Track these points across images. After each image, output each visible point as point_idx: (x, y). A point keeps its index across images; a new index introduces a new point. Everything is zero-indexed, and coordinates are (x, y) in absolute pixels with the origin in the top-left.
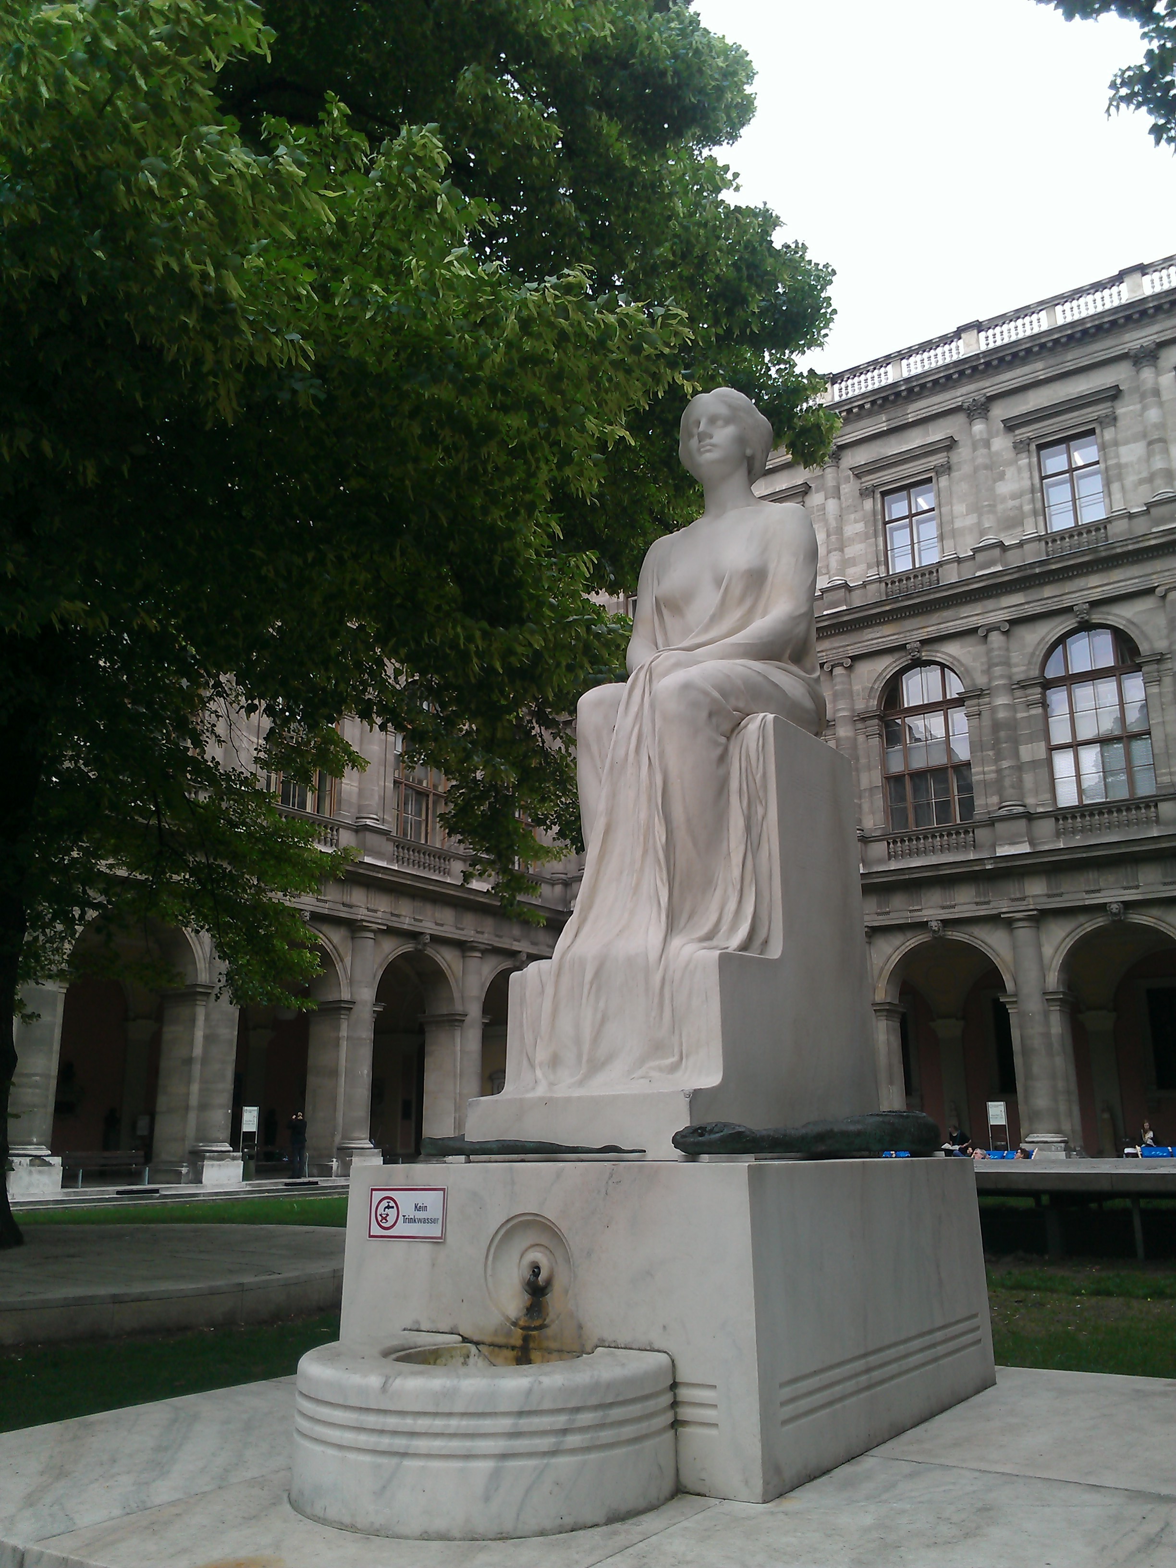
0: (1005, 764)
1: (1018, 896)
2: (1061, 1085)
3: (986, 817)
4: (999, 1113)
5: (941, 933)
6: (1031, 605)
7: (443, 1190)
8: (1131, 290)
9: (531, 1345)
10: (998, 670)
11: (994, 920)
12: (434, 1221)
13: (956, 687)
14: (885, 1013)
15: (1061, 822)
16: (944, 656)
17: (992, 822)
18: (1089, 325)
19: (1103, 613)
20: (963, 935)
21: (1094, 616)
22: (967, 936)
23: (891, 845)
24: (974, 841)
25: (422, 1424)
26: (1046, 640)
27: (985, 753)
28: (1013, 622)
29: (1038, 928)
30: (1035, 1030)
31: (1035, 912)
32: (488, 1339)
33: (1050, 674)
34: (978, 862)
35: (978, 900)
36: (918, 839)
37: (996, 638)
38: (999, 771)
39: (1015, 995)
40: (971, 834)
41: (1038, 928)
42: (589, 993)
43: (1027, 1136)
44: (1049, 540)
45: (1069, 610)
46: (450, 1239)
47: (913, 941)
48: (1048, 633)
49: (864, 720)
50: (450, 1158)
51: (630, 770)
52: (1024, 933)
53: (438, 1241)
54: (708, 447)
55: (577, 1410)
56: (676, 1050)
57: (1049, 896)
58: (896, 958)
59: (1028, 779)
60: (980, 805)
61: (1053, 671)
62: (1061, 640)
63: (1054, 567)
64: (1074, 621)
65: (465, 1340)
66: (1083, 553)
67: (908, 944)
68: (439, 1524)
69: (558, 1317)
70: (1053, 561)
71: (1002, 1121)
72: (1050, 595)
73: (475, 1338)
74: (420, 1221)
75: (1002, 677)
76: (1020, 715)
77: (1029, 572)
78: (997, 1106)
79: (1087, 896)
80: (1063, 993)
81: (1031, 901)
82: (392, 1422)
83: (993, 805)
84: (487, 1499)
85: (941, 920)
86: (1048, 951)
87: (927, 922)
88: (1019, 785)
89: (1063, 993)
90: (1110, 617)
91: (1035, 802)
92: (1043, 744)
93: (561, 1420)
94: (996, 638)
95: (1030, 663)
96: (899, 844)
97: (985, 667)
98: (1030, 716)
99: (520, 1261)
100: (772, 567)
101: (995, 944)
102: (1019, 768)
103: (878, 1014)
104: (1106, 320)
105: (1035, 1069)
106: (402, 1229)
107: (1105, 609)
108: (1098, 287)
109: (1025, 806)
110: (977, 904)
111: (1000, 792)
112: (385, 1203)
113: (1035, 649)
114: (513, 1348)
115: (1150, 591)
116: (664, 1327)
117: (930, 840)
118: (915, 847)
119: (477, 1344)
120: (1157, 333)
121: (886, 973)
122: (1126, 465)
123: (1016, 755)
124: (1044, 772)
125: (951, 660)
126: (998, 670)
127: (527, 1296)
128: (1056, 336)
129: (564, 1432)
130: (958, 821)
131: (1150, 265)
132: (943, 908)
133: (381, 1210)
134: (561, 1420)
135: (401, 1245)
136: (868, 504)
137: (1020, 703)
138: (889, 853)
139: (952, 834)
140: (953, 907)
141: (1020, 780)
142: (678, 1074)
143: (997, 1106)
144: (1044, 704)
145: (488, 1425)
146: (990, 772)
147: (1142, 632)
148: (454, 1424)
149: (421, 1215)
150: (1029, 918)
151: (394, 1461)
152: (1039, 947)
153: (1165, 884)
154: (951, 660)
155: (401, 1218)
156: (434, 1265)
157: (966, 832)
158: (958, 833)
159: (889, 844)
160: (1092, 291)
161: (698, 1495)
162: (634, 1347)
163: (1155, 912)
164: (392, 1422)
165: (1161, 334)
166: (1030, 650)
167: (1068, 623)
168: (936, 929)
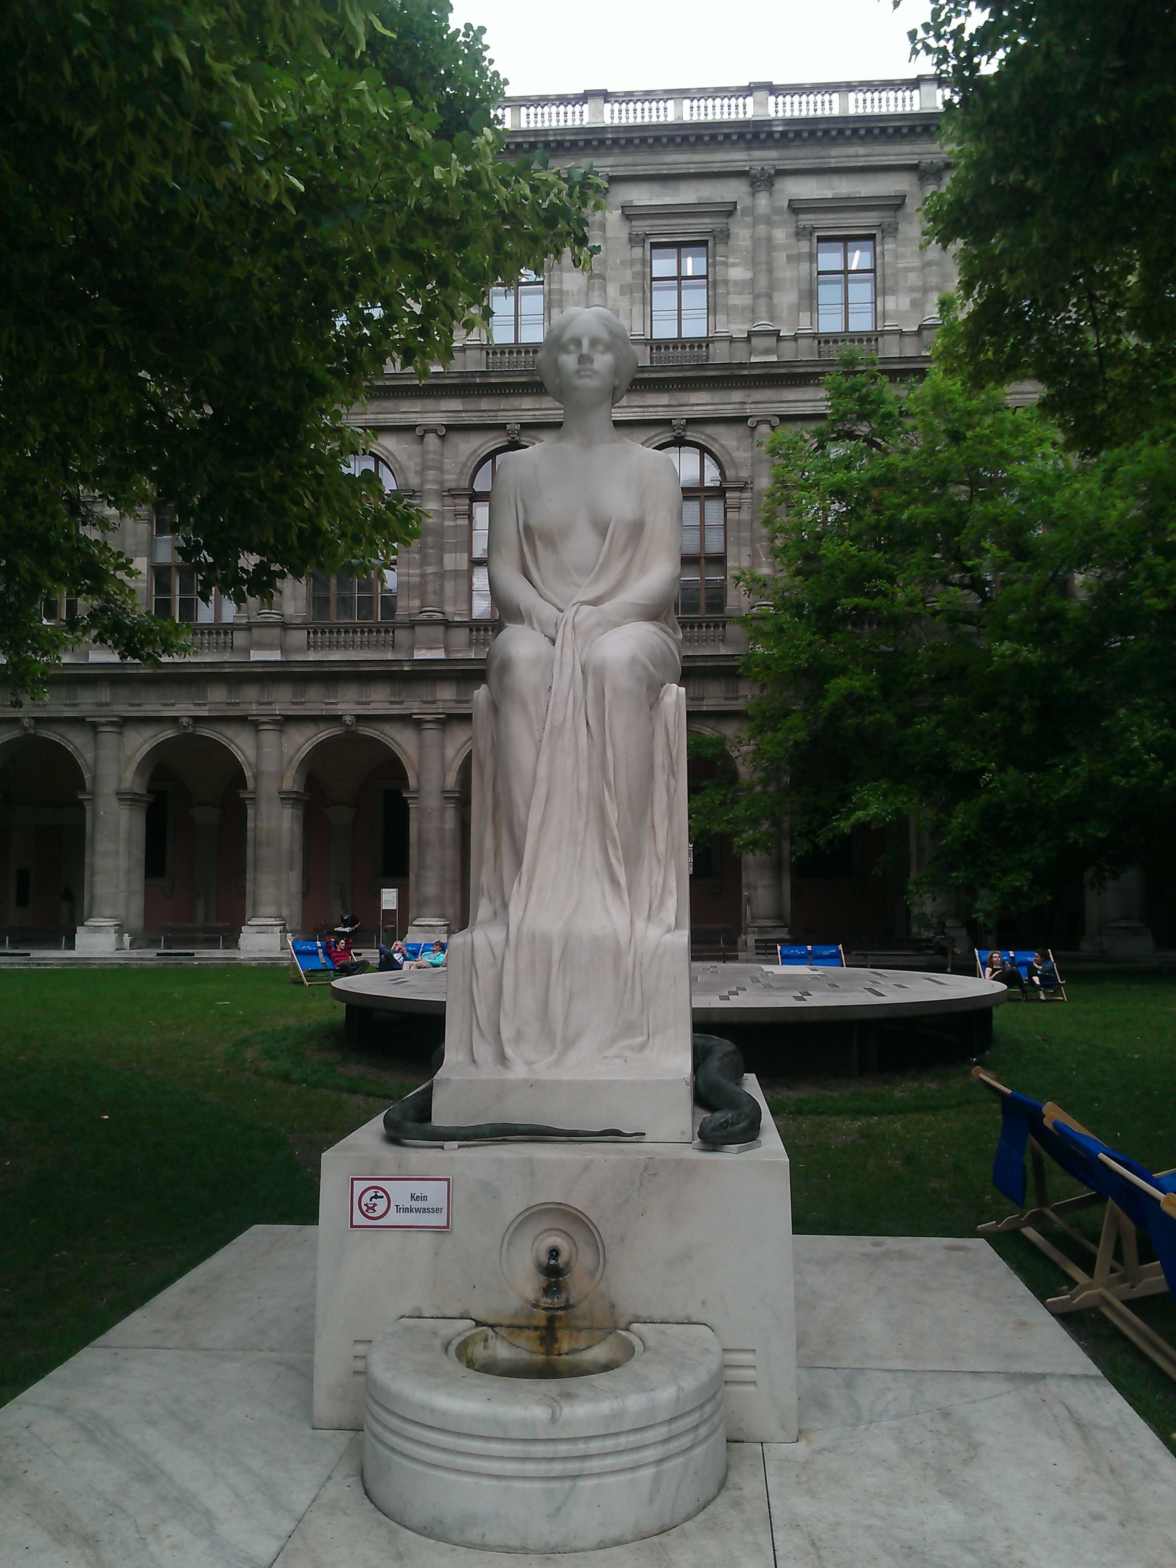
0: (430, 570)
1: (430, 699)
3: (407, 620)
4: (391, 899)
6: (469, 414)
7: (448, 1180)
8: (592, 114)
9: (557, 1325)
10: (431, 474)
11: (405, 719)
12: (438, 1210)
14: (292, 802)
15: (474, 633)
16: (379, 448)
17: (412, 625)
18: (551, 138)
19: (702, 433)
21: (523, 439)
22: (378, 733)
23: (312, 635)
24: (393, 641)
25: (594, 1446)
26: (479, 452)
27: (411, 555)
28: (450, 428)
31: (443, 716)
32: (506, 1321)
33: (477, 488)
34: (397, 663)
36: (339, 632)
37: (431, 440)
38: (423, 576)
39: (417, 792)
42: (558, 972)
44: (491, 352)
45: (502, 427)
46: (456, 1227)
47: (325, 733)
50: (447, 1144)
52: (431, 735)
54: (589, 373)
55: (701, 1406)
56: (645, 1029)
57: (457, 702)
59: (449, 587)
62: (492, 455)
63: (493, 381)
64: (505, 439)
65: (478, 1324)
66: (521, 373)
67: (320, 735)
68: (614, 1532)
69: (586, 1297)
70: (493, 374)
71: (394, 907)
72: (486, 408)
73: (491, 1321)
75: (434, 481)
76: (447, 523)
77: (470, 380)
78: (390, 893)
80: (460, 792)
81: (440, 704)
82: (564, 1449)
84: (651, 1501)
86: (450, 752)
87: (341, 716)
88: (440, 592)
89: (460, 792)
91: (453, 611)
92: (466, 555)
93: (695, 1417)
94: (431, 440)
95: (461, 473)
96: (319, 635)
97: (419, 468)
98: (456, 526)
99: (533, 1243)
101: (403, 742)
102: (442, 575)
103: (284, 802)
104: (568, 138)
105: (429, 861)
106: (393, 1218)
108: (563, 100)
110: (392, 703)
111: (423, 596)
112: (371, 1193)
114: (536, 1328)
116: (703, 1303)
117: (351, 635)
118: (335, 640)
119: (492, 1326)
120: (611, 166)
122: (568, 292)
123: (441, 562)
124: (464, 583)
125: (386, 454)
126: (431, 474)
127: (542, 1278)
128: (519, 140)
129: (696, 1427)
130: (379, 620)
131: (613, 94)
132: (358, 703)
133: (366, 1199)
134: (695, 1417)
135: (397, 1234)
136: (637, 252)
137: (449, 511)
138: (308, 643)
139: (372, 632)
140: (368, 703)
141: (442, 588)
142: (647, 1052)
143: (390, 893)
144: (470, 517)
146: (414, 575)
148: (623, 1441)
149: (416, 1204)
151: (568, 1484)
152: (443, 747)
153: (726, 699)
154: (386, 454)
155: (393, 1208)
156: (437, 1254)
157: (387, 631)
158: (378, 632)
159: (309, 633)
160: (557, 103)
161: (737, 1441)
162: (671, 1321)
163: (62, 729)
164: (564, 1449)
165: (615, 169)
166: (462, 459)
168: (349, 723)
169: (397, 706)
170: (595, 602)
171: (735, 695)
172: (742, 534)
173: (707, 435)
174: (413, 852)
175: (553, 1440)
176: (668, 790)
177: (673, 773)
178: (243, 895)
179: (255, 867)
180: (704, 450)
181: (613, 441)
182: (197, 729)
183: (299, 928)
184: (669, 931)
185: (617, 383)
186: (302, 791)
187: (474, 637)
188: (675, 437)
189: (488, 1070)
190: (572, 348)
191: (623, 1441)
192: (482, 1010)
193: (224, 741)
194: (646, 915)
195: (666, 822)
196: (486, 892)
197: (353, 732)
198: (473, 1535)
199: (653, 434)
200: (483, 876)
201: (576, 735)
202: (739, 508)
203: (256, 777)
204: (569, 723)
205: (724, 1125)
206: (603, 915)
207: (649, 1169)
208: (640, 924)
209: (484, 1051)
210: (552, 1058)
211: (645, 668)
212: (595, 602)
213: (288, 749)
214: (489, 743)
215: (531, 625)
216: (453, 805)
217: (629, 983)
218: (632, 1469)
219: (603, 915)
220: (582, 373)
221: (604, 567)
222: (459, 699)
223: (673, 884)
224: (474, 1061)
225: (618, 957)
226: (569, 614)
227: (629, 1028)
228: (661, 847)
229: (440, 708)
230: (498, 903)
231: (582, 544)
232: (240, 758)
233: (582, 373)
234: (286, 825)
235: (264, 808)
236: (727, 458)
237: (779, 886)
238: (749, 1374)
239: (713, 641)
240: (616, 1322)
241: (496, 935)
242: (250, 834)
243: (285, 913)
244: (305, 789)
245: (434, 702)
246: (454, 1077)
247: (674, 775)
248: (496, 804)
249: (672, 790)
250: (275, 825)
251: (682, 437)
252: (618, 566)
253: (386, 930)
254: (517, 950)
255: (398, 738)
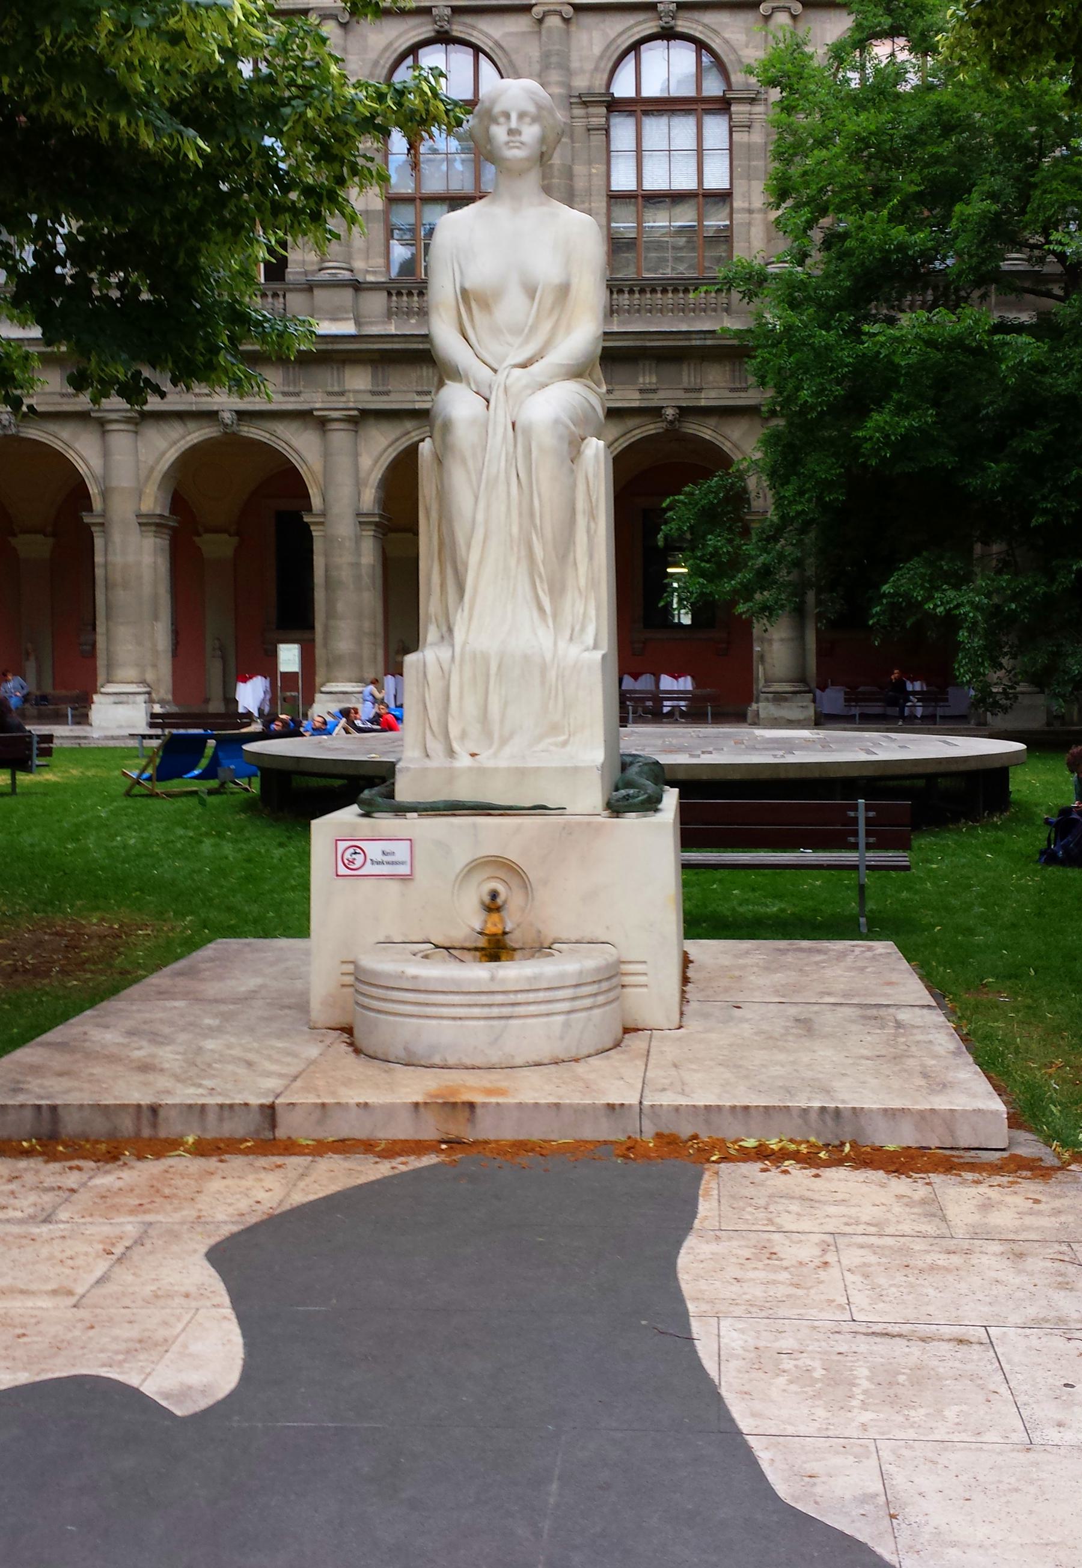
1: (336, 389)
2: (367, 625)
3: (302, 279)
5: (235, 428)
11: (303, 416)
12: (403, 863)
13: (713, 87)
14: (153, 528)
15: (394, 298)
17: (310, 287)
19: (464, 24)
20: (263, 433)
25: (520, 997)
29: (356, 432)
30: (344, 559)
35: (286, 389)
39: (323, 514)
40: (281, 300)
41: (356, 432)
43: (323, 685)
45: (426, 11)
48: (398, 37)
49: (586, 104)
50: (409, 815)
51: (502, 488)
52: (340, 438)
53: (405, 879)
54: (518, 144)
55: (600, 981)
58: (172, 455)
60: (295, 261)
61: (623, 87)
62: (635, 47)
65: (437, 947)
73: (446, 945)
74: (388, 863)
79: (417, 398)
82: (499, 999)
83: (312, 263)
85: (236, 412)
86: (366, 462)
89: (381, 516)
90: (475, 33)
93: (593, 989)
100: (575, 282)
101: (302, 447)
105: (340, 607)
106: (369, 869)
107: (468, 19)
109: (352, 271)
113: (380, 56)
115: (527, 9)
119: (447, 948)
121: (157, 475)
129: (595, 995)
133: (347, 855)
134: (593, 989)
142: (568, 748)
145: (560, 994)
147: (510, 61)
148: (541, 995)
150: (349, 420)
151: (503, 1022)
152: (356, 455)
153: (732, 390)
164: (499, 999)
166: (372, 55)
167: (423, 29)
169: (292, 399)
170: (524, 366)
171: (744, 385)
172: (754, 163)
173: (705, 26)
174: (319, 595)
175: (493, 992)
176: (588, 531)
177: (592, 516)
178: (92, 654)
179: (108, 617)
180: (701, 46)
181: (542, 204)
182: (21, 429)
183: (170, 697)
184: (587, 649)
185: (544, 149)
186: (167, 514)
187: (394, 304)
188: (662, 28)
189: (439, 760)
190: (502, 120)
191: (541, 995)
192: (433, 714)
193: (58, 445)
194: (568, 637)
195: (586, 560)
196: (434, 620)
197: (234, 433)
198: (437, 1060)
199: (632, 22)
200: (430, 604)
201: (508, 485)
202: (749, 127)
203: (105, 494)
204: (502, 475)
205: (627, 797)
206: (535, 637)
207: (567, 830)
208: (562, 644)
209: (436, 747)
210: (491, 751)
211: (567, 427)
212: (524, 366)
213: (147, 456)
214: (434, 492)
215: (469, 384)
216: (372, 533)
217: (553, 692)
218: (548, 1015)
219: (535, 637)
220: (511, 144)
221: (534, 329)
222: (376, 389)
223: (592, 613)
224: (428, 756)
225: (544, 670)
226: (501, 377)
227: (555, 729)
228: (582, 582)
229: (352, 402)
230: (444, 629)
231: (513, 306)
232: (82, 468)
233: (511, 144)
234: (147, 559)
235: (117, 537)
236: (732, 57)
237: (801, 638)
238: (642, 979)
239: (715, 310)
240: (542, 943)
241: (444, 653)
242: (99, 572)
243: (150, 676)
244: (170, 513)
245: (342, 394)
246: (412, 766)
247: (594, 519)
248: (441, 544)
249: (592, 531)
250: (133, 560)
251: (672, 28)
252: (546, 326)
253: (285, 699)
254: (461, 665)
255: (295, 442)
